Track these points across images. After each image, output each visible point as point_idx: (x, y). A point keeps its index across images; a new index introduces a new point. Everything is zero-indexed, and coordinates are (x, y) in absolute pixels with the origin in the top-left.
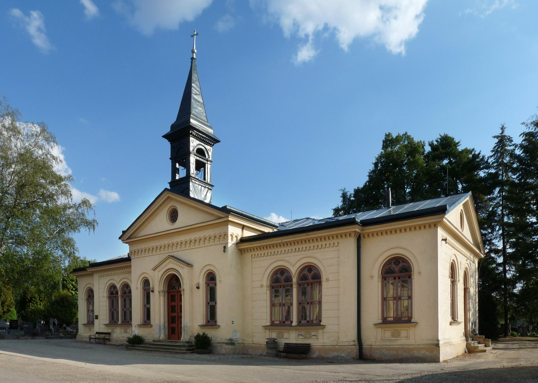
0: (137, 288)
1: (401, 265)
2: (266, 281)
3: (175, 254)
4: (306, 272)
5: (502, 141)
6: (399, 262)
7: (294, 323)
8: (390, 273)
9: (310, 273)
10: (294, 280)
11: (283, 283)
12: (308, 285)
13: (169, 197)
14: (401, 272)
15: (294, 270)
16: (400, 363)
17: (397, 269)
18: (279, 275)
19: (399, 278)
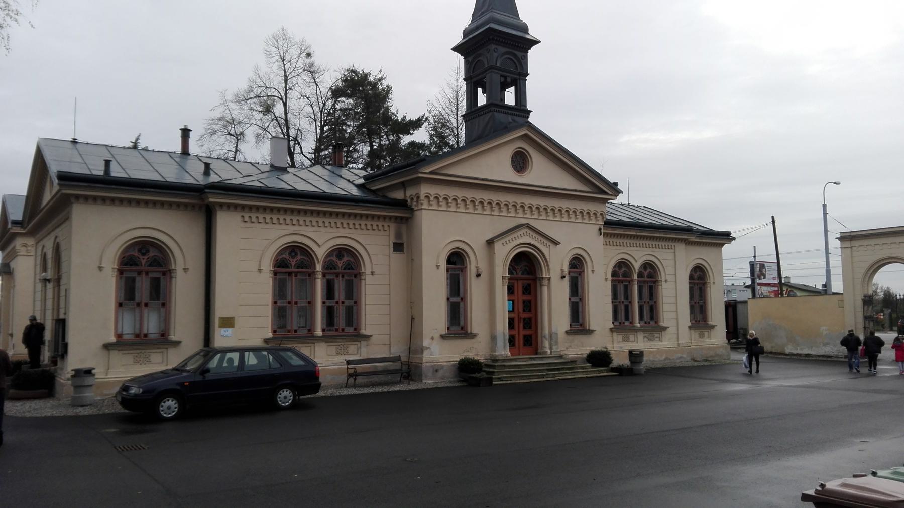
0: (438, 267)
1: (345, 259)
2: (111, 263)
3: (532, 223)
4: (286, 256)
5: (405, 117)
6: (296, 254)
7: (319, 332)
8: (131, 265)
9: (340, 259)
10: (319, 268)
11: (646, 279)
12: (337, 276)
13: (526, 135)
14: (298, 268)
15: (637, 266)
16: (24, 419)
17: (340, 264)
18: (334, 258)
19: (147, 274)
